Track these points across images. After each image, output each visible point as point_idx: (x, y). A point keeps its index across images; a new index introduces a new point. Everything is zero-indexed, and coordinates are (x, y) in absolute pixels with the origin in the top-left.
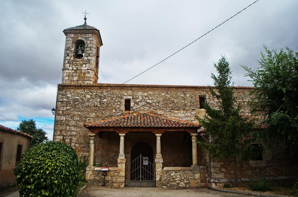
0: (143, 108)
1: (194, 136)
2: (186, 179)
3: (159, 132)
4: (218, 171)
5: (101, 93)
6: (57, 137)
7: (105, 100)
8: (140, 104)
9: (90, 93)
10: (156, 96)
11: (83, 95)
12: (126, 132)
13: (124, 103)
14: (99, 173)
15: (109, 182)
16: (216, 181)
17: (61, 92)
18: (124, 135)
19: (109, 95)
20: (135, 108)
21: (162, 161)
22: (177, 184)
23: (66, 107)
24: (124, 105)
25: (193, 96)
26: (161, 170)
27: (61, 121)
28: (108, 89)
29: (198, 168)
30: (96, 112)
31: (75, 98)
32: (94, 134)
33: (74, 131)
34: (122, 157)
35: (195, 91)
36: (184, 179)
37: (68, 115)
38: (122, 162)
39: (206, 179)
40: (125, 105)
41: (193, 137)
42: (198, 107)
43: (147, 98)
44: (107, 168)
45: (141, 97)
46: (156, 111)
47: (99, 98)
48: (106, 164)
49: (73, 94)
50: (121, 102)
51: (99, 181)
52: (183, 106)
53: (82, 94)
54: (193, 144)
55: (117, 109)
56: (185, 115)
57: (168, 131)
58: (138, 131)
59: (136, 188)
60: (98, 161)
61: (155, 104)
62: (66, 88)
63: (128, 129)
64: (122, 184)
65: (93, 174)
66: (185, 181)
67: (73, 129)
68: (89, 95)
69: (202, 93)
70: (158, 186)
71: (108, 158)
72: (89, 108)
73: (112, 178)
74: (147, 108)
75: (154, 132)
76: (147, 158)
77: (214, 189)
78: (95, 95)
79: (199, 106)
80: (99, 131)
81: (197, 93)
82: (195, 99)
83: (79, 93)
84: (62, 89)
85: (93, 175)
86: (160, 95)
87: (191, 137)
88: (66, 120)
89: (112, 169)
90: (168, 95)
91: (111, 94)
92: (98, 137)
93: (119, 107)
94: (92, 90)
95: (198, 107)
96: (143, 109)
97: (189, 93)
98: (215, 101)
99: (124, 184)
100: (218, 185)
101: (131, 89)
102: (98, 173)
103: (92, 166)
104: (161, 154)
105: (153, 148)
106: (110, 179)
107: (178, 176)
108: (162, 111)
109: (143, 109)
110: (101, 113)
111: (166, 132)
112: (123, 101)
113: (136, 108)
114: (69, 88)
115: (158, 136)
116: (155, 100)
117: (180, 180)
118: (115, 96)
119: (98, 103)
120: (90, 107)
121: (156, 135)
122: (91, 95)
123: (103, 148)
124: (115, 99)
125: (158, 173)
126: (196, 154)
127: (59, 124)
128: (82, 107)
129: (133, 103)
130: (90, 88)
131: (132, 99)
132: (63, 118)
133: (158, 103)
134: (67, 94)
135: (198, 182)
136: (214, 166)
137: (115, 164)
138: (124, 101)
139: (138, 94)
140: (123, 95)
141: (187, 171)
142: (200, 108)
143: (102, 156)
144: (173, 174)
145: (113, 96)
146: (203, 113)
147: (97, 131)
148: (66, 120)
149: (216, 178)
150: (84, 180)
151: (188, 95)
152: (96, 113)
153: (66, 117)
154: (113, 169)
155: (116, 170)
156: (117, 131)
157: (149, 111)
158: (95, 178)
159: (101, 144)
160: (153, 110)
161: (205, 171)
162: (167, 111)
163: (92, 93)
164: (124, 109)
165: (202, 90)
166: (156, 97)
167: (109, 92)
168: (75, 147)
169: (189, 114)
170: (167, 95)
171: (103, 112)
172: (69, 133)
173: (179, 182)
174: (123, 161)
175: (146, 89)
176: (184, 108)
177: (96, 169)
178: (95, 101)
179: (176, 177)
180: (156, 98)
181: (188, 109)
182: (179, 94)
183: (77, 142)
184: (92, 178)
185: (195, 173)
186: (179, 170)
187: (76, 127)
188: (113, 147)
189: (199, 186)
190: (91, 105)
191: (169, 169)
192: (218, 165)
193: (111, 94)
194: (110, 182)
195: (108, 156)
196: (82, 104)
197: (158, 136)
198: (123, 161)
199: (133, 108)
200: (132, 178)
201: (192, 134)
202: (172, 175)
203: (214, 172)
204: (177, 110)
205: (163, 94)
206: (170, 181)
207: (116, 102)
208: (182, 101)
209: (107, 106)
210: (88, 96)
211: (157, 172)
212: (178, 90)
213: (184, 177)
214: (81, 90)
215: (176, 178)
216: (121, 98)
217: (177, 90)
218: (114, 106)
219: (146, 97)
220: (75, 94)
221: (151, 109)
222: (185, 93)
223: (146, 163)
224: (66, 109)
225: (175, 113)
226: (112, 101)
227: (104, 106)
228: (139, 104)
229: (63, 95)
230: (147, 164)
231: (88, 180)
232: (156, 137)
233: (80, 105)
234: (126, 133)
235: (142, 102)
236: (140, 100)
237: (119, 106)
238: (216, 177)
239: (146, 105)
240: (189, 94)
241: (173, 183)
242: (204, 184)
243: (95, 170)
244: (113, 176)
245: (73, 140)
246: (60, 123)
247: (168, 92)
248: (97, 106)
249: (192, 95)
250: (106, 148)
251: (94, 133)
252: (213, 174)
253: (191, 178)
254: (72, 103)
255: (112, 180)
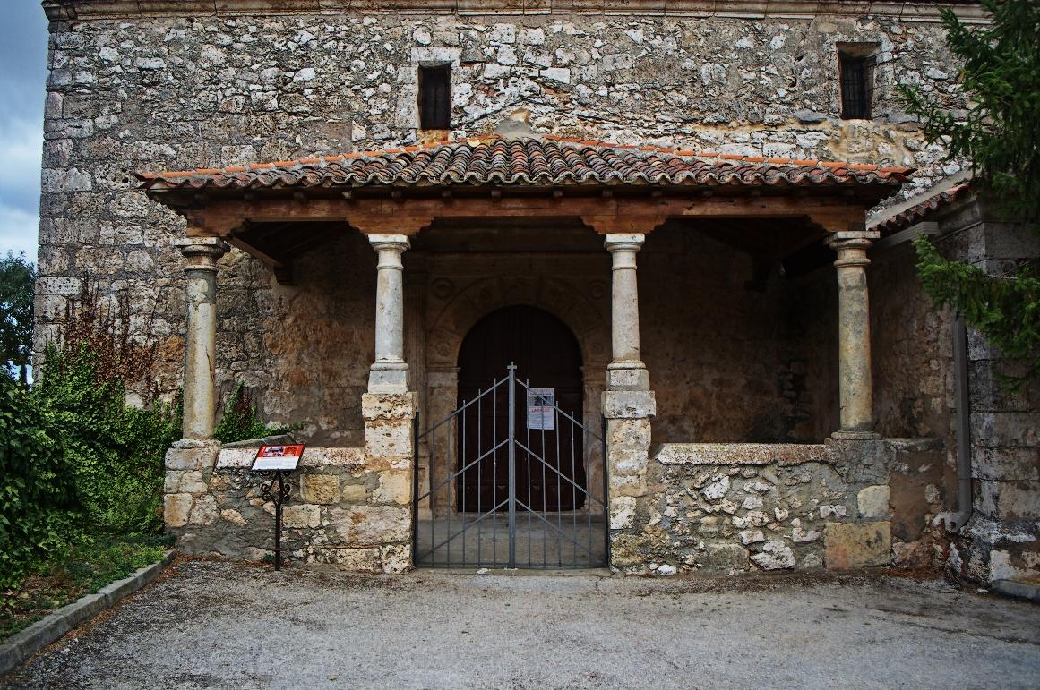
0: (524, 114)
1: (854, 247)
2: (802, 518)
3: (628, 225)
4: (1025, 468)
5: (282, 33)
6: (50, 283)
7: (307, 73)
8: (507, 91)
9: (223, 36)
10: (598, 43)
11: (186, 48)
12: (417, 225)
13: (415, 89)
14: (246, 485)
15: (310, 539)
16: (1015, 539)
17: (63, 39)
18: (403, 238)
19: (331, 44)
20: (475, 112)
21: (646, 405)
22: (747, 552)
23: (93, 118)
24: (414, 98)
25: (807, 47)
26: (644, 460)
27: (71, 194)
28: (319, 8)
29: (881, 448)
30: (258, 138)
31: (141, 69)
32: (212, 241)
33: (140, 247)
34: (388, 381)
35: (819, 19)
36: (791, 517)
37: (103, 160)
38: (389, 415)
39: (928, 517)
40: (423, 101)
41: (849, 256)
42: (833, 105)
43: (545, 60)
44: (291, 450)
45: (513, 49)
46: (595, 129)
47: (274, 63)
48: (319, 428)
49: (127, 45)
50: (399, 80)
51: (247, 537)
52: (747, 99)
53: (177, 42)
54: (845, 297)
55: (373, 120)
56: (760, 155)
57: (686, 212)
58: (491, 213)
59: (484, 579)
60: (278, 411)
61: (590, 91)
62: (92, 13)
63: (429, 204)
64: (392, 552)
65: (210, 492)
66: (796, 535)
67: (136, 236)
68: (217, 46)
69: (858, 27)
70: (626, 561)
71: (331, 395)
72: (220, 120)
73: (329, 517)
74: (543, 114)
75: (596, 225)
76: (551, 392)
77: (1004, 586)
78: (252, 49)
79: (837, 104)
80: (240, 221)
81: (825, 28)
82: (815, 60)
83: (161, 36)
84: (71, 18)
85: (210, 499)
86: (617, 37)
87: (834, 254)
88: (97, 188)
89: (326, 461)
90: (663, 37)
91: (338, 40)
92: (274, 280)
93: (384, 112)
94: (234, 19)
95: (833, 105)
96: (520, 117)
97: (781, 26)
98: (929, 73)
99: (407, 553)
100: (1028, 559)
101: (453, 8)
102: (244, 482)
103: (201, 443)
104: (643, 365)
105: (579, 338)
106: (315, 524)
107: (749, 502)
108: (628, 132)
109: (520, 117)
110: (288, 146)
111: (676, 221)
112: (409, 76)
113: (485, 116)
114: (103, 13)
115: (625, 246)
116: (593, 71)
117: (763, 527)
118: (361, 49)
119: (267, 87)
120: (224, 113)
121: (610, 238)
122: (229, 47)
123: (305, 338)
124: (362, 64)
125: (624, 481)
126: (867, 361)
127: (57, 210)
128: (179, 117)
129: (468, 87)
130: (223, 9)
131: (458, 61)
132: (82, 180)
133: (609, 85)
134: (99, 43)
135: (879, 538)
136: (1002, 436)
137: (351, 427)
138: (415, 77)
139: (496, 35)
140: (406, 41)
141: (808, 466)
142: (846, 116)
143: (300, 383)
144: (718, 485)
145: (350, 47)
146: (862, 140)
147: (232, 219)
148: (97, 188)
149: (1011, 514)
150: (158, 532)
151: (778, 42)
152: (258, 146)
153: (92, 174)
154: (338, 461)
155: (353, 467)
156: (355, 220)
157: (556, 130)
158: (225, 513)
159: (290, 320)
160: (580, 127)
161: (923, 469)
162: (661, 127)
163: (234, 35)
164: (415, 121)
165: (859, 9)
166: (594, 51)
167: (330, 29)
168: (150, 336)
169: (786, 147)
170: (657, 41)
171: (298, 140)
172: (116, 261)
173: (759, 536)
174: (400, 410)
175: (537, 7)
176: (756, 109)
177: (229, 457)
178: (249, 82)
179: (739, 508)
180: (598, 56)
181: (774, 117)
182: (727, 33)
183: (162, 311)
184: (207, 517)
185: (857, 484)
186: (755, 466)
187: (154, 224)
188: (356, 336)
189: (882, 562)
190: (230, 103)
191: (696, 459)
192: (1027, 430)
193: (338, 40)
194: (318, 540)
195: (332, 384)
196: (182, 101)
197: (625, 246)
198: (400, 410)
199: (466, 114)
200: (477, 494)
201: (841, 234)
202: (712, 492)
203: (1002, 480)
204: (715, 125)
205: (638, 35)
206: (702, 529)
207: (372, 84)
208: (745, 76)
209: (320, 107)
210: (214, 54)
211: (617, 473)
212: (722, 11)
213: (790, 508)
214: (170, 22)
215: (741, 510)
216: (400, 59)
217: (715, 11)
218: (356, 106)
219: (538, 49)
220: (138, 43)
221: (571, 120)
222: (758, 26)
223: (543, 418)
224: (94, 126)
225: (705, 143)
226: (348, 78)
227: (301, 108)
228: (502, 89)
229: (73, 53)
230: (550, 424)
231: (183, 529)
232: (605, 256)
233: (167, 105)
234: (418, 229)
235: (513, 79)
236: (505, 69)
237: (385, 107)
238: (1015, 509)
239: (537, 94)
240: (783, 37)
241: (718, 546)
242: (911, 546)
243: (219, 465)
244: (336, 500)
245: (139, 297)
246: (65, 209)
247: (665, 22)
248: (261, 108)
249: (802, 43)
250: (318, 342)
251: (209, 232)
252: (987, 489)
253: (832, 513)
254: (123, 93)
255: (328, 529)
